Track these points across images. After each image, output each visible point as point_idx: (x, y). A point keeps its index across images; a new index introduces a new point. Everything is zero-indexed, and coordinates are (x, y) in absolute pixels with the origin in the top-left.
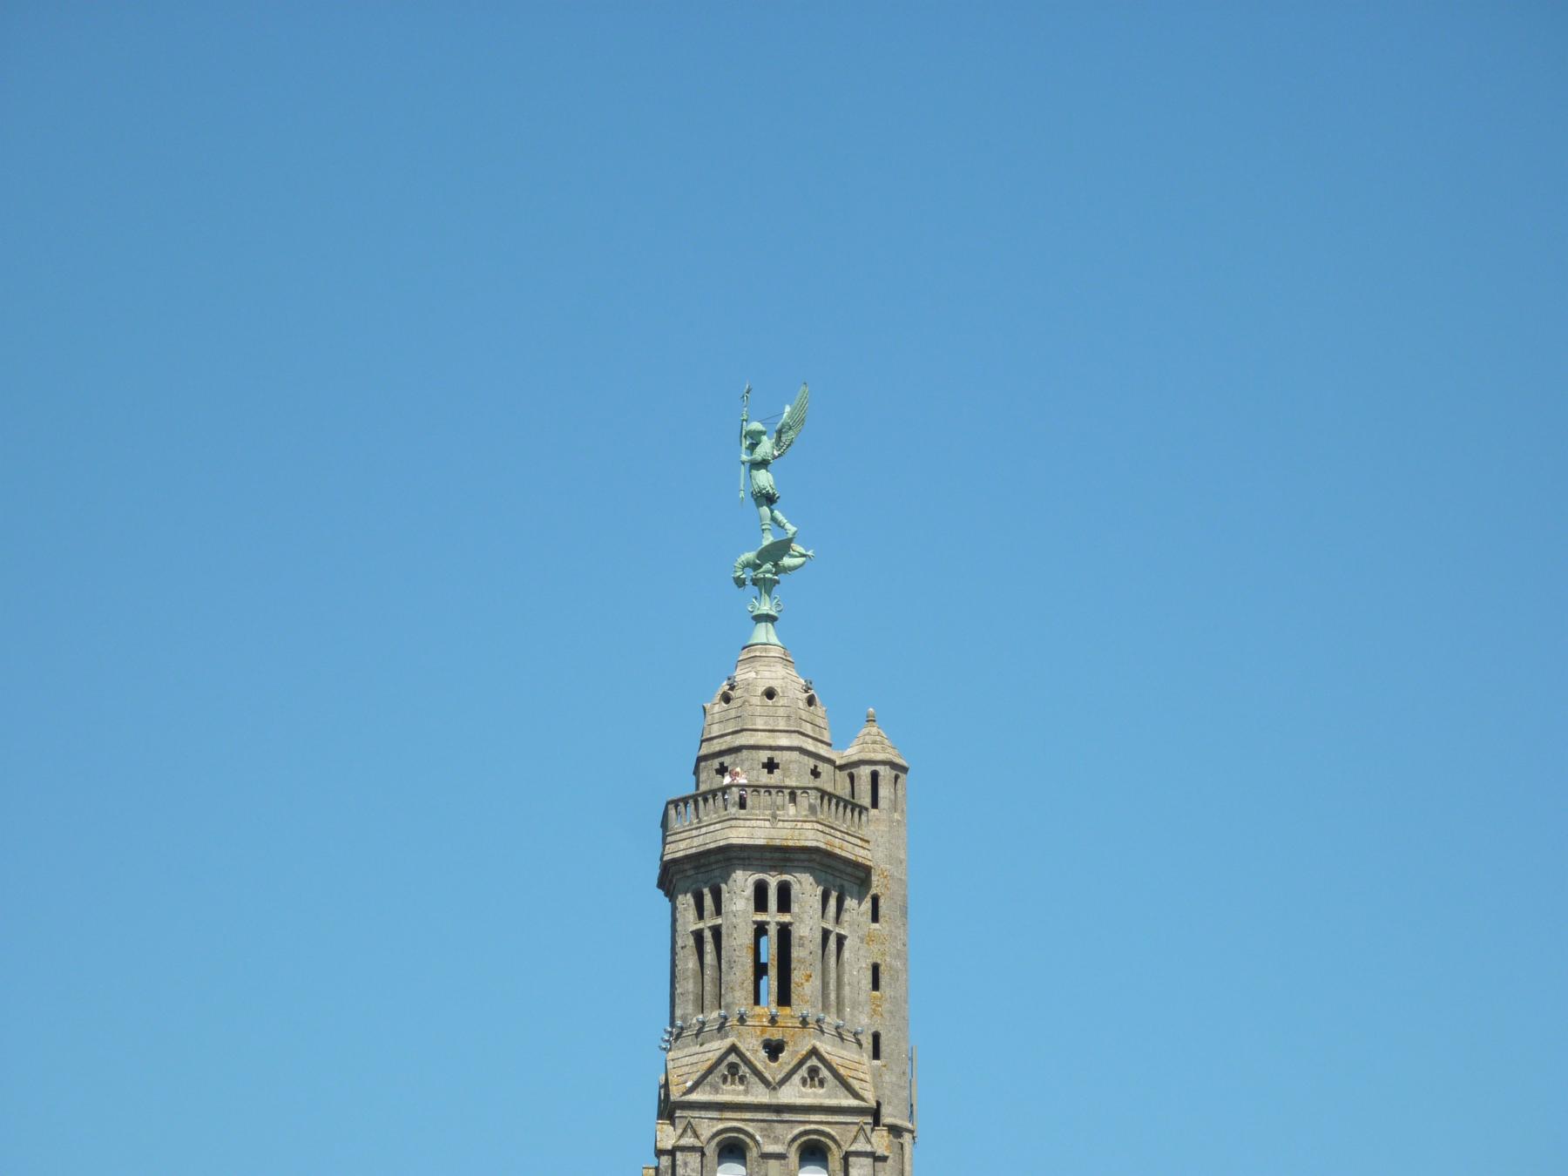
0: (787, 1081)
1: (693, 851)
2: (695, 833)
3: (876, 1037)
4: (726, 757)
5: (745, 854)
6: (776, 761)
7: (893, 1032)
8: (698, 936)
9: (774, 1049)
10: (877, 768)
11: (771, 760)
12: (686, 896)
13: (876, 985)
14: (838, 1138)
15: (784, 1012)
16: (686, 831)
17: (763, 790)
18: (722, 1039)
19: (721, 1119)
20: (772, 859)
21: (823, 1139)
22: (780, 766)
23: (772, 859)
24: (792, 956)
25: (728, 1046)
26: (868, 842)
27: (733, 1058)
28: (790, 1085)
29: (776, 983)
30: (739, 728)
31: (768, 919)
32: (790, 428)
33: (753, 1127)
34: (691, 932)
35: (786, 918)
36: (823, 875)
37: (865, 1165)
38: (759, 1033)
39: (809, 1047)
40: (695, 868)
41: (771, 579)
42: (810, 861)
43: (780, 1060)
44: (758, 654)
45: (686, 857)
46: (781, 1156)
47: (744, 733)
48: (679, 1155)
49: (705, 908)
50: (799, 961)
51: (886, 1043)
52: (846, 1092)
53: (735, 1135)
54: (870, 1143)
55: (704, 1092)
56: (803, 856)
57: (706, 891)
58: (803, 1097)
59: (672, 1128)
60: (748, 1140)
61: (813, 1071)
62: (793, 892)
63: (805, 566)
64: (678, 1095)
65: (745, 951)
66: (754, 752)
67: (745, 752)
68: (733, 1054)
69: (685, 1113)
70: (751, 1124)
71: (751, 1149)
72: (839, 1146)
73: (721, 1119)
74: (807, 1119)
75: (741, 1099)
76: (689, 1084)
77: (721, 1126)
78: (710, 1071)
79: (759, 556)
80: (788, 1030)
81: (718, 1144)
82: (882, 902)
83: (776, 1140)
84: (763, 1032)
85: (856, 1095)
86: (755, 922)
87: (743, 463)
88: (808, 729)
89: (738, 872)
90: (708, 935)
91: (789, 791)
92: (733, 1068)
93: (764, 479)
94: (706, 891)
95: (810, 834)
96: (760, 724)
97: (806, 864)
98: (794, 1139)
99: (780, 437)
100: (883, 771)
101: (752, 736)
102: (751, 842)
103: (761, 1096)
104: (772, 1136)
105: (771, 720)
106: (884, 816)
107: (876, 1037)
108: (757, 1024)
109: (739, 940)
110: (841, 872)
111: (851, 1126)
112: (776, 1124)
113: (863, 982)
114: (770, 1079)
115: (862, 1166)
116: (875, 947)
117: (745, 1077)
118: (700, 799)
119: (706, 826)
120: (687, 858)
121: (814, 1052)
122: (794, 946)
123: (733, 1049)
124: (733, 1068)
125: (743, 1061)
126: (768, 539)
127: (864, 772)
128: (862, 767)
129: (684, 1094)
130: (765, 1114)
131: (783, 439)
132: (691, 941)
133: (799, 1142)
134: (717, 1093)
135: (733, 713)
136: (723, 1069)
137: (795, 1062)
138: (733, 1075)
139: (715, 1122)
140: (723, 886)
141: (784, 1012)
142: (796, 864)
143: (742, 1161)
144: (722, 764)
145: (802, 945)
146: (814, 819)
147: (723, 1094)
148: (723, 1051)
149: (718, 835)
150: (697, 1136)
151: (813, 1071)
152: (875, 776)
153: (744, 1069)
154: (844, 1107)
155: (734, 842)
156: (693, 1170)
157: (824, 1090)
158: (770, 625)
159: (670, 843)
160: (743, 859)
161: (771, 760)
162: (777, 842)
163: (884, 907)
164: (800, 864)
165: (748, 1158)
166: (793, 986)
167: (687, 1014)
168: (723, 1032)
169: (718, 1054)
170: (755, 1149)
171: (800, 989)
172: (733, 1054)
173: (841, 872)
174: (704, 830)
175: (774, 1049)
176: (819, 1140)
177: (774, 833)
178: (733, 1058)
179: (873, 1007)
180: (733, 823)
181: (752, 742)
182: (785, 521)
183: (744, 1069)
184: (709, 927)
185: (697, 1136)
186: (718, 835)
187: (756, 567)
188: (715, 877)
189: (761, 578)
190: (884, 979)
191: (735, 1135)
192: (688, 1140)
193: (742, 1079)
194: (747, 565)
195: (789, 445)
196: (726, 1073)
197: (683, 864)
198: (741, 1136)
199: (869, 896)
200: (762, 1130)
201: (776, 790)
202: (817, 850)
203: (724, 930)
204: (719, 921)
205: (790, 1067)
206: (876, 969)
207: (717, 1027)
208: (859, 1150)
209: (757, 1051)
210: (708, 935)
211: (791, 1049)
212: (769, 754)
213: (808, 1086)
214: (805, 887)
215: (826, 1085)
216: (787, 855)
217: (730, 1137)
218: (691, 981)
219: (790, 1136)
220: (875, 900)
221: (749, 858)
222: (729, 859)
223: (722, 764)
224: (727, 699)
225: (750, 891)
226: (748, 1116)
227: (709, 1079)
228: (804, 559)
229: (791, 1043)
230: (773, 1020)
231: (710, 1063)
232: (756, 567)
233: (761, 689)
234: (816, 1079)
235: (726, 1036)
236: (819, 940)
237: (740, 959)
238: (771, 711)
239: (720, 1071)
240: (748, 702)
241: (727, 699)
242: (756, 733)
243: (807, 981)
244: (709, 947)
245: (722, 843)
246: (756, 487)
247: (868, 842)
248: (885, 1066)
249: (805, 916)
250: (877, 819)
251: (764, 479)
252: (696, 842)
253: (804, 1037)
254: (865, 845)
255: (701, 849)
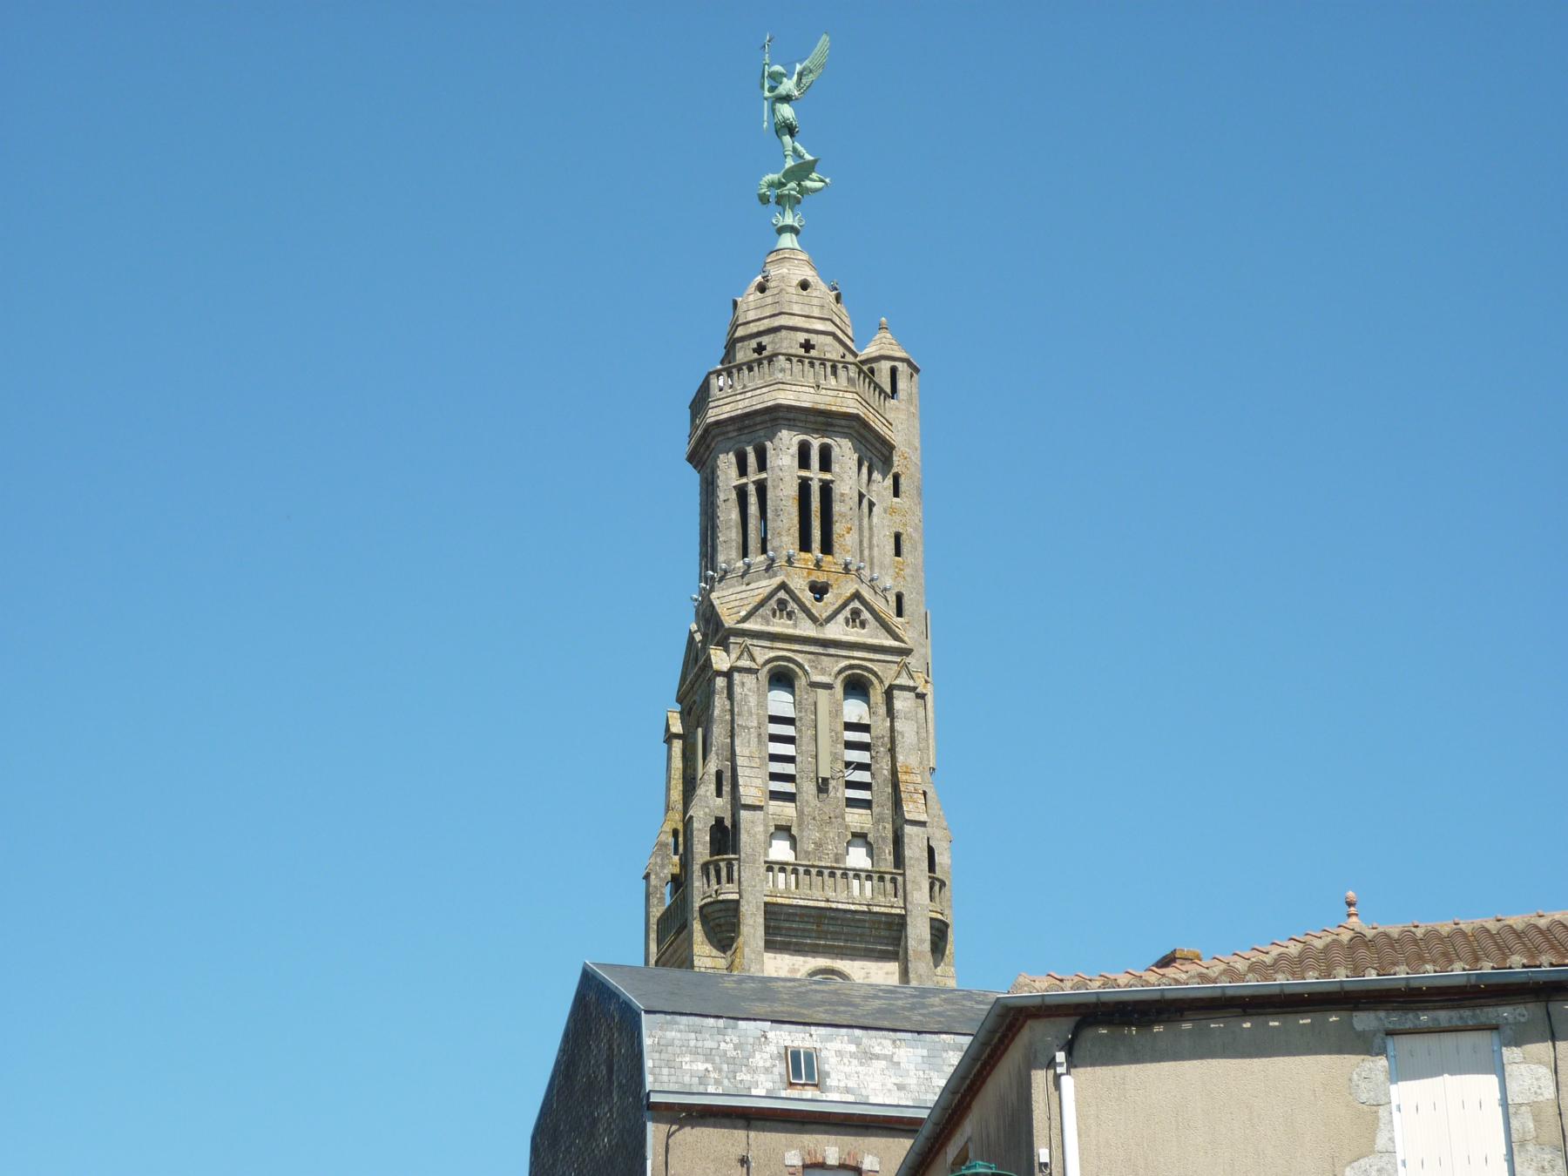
0: (832, 619)
1: (739, 412)
2: (739, 397)
3: (899, 597)
4: (765, 337)
5: (791, 416)
6: (812, 342)
7: (914, 594)
8: (742, 493)
9: (819, 590)
10: (896, 364)
11: (807, 341)
12: (728, 454)
13: (898, 553)
14: (880, 673)
15: (827, 559)
16: (730, 396)
17: (807, 361)
18: (770, 578)
19: (772, 648)
20: (815, 423)
21: (866, 674)
22: (816, 348)
23: (815, 423)
24: (834, 510)
25: (779, 583)
26: (891, 425)
27: (782, 594)
28: (836, 623)
29: (819, 533)
30: (777, 312)
31: (812, 476)
32: (811, 71)
33: (802, 658)
34: (734, 487)
35: (828, 476)
36: (859, 445)
37: (908, 699)
38: (805, 574)
39: (852, 590)
40: (740, 429)
41: (795, 197)
42: (848, 427)
43: (825, 600)
44: (786, 256)
45: (731, 419)
46: (828, 687)
47: (783, 316)
48: (736, 676)
49: (749, 464)
50: (840, 515)
51: (909, 603)
52: (886, 634)
53: (785, 664)
54: (913, 678)
55: (756, 623)
56: (843, 422)
57: (750, 449)
58: (847, 635)
59: (725, 654)
60: (797, 670)
61: (856, 613)
62: (833, 454)
63: (768, 252)
64: (733, 622)
65: (791, 501)
66: (792, 332)
67: (784, 333)
68: (783, 591)
69: (740, 640)
70: (800, 655)
71: (800, 678)
72: (881, 682)
73: (772, 648)
74: (851, 655)
75: (790, 631)
76: (743, 613)
77: (772, 654)
78: (762, 604)
79: (784, 176)
80: (832, 574)
81: (770, 670)
82: (902, 480)
83: (823, 672)
84: (809, 574)
85: (896, 637)
86: (799, 477)
87: (766, 99)
88: (838, 321)
89: (783, 431)
90: (752, 489)
91: (831, 363)
92: (782, 604)
93: (786, 111)
94: (750, 449)
95: (852, 403)
96: (796, 309)
97: (846, 430)
98: (840, 672)
99: (801, 79)
100: (901, 367)
101: (790, 319)
102: (798, 404)
103: (807, 629)
104: (819, 667)
105: (806, 308)
106: (903, 406)
107: (899, 597)
108: (803, 566)
109: (784, 494)
110: (872, 445)
111: (892, 665)
112: (823, 657)
113: (887, 547)
114: (817, 615)
115: (905, 699)
116: (897, 518)
117: (794, 612)
118: (744, 367)
119: (752, 390)
120: (732, 420)
121: (857, 596)
122: (836, 501)
123: (783, 586)
124: (782, 604)
125: (791, 597)
126: (790, 163)
127: (885, 366)
128: (883, 362)
129: (738, 622)
130: (813, 647)
131: (804, 81)
132: (734, 496)
133: (844, 675)
134: (768, 625)
135: (769, 300)
136: (773, 603)
137: (840, 602)
138: (781, 611)
139: (766, 650)
140: (768, 444)
141: (827, 559)
142: (836, 429)
143: (790, 690)
144: (759, 344)
145: (843, 501)
146: (854, 390)
147: (773, 625)
148: (774, 587)
149: (766, 397)
150: (753, 659)
151: (856, 613)
152: (894, 371)
153: (792, 606)
154: (886, 647)
155: (783, 402)
156: (749, 690)
157: (866, 630)
158: (794, 235)
159: (713, 408)
160: (789, 420)
161: (807, 341)
162: (822, 407)
163: (905, 485)
164: (840, 430)
165: (796, 686)
166: (835, 537)
167: (731, 559)
168: (771, 572)
169: (769, 590)
170: (803, 677)
171: (842, 539)
172: (783, 591)
173: (872, 445)
174: (749, 394)
175: (819, 590)
176: (863, 675)
177: (818, 398)
178: (782, 594)
179: (897, 570)
180: (781, 386)
181: (790, 323)
182: (804, 151)
183: (792, 606)
184: (753, 482)
185: (753, 659)
186: (766, 397)
187: (782, 185)
188: (760, 437)
189: (786, 195)
190: (905, 548)
191: (785, 664)
192: (745, 663)
193: (790, 615)
194: (771, 185)
195: (809, 86)
196: (776, 607)
197: (726, 426)
198: (791, 665)
199: (891, 474)
200: (810, 661)
201: (819, 362)
202: (856, 417)
203: (769, 484)
204: (764, 475)
205: (837, 606)
206: (898, 537)
207: (764, 568)
208: (903, 684)
209: (804, 590)
210: (752, 489)
211: (835, 591)
212: (805, 336)
213: (850, 626)
214: (844, 451)
215: (867, 626)
216: (830, 420)
217: (779, 666)
218: (734, 530)
219: (837, 669)
220: (896, 478)
221: (794, 420)
222: (775, 419)
223: (759, 344)
224: (762, 288)
225: (794, 449)
226: (797, 647)
227: (761, 611)
228: (823, 184)
229: (835, 586)
230: (818, 565)
231: (761, 597)
232: (782, 185)
233: (795, 282)
234: (857, 621)
235: (775, 575)
236: (857, 499)
237: (788, 509)
238: (806, 300)
239: (771, 605)
240: (785, 290)
241: (762, 288)
242: (793, 317)
243: (848, 533)
244: (753, 500)
245: (769, 404)
246: (780, 117)
247: (891, 425)
248: (908, 623)
249: (845, 476)
250: (897, 408)
251: (786, 111)
252: (741, 405)
253: (847, 582)
254: (890, 427)
255: (748, 410)
